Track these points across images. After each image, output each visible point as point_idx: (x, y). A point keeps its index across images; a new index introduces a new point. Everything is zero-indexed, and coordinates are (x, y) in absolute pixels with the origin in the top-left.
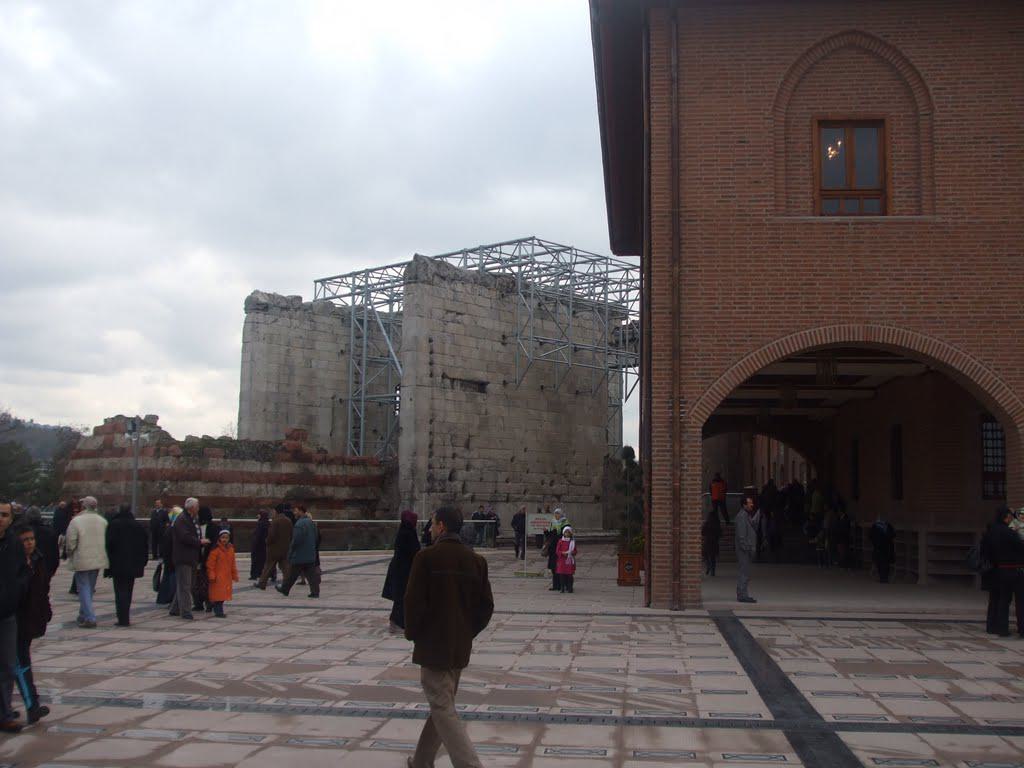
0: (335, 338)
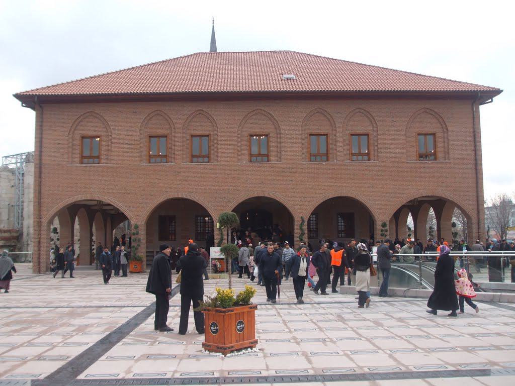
0: (10, 181)
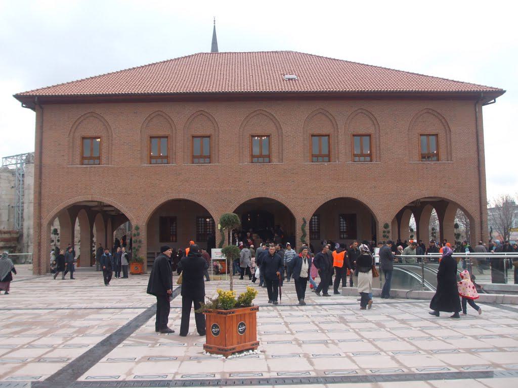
0: (10, 182)
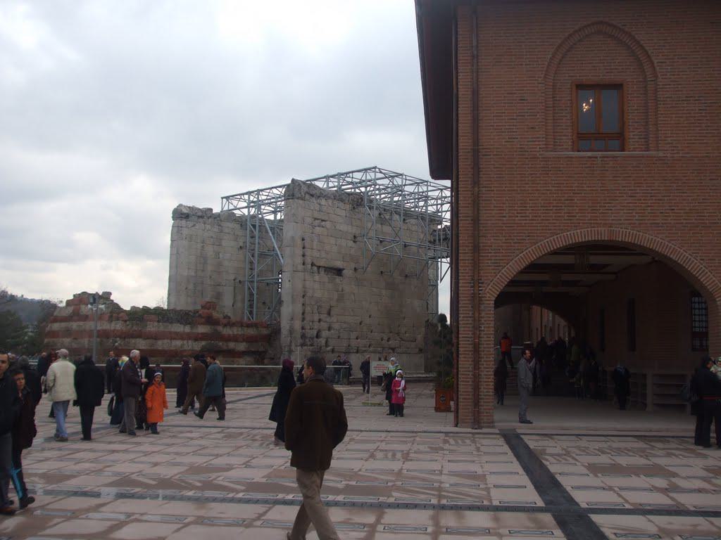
0: (236, 238)
